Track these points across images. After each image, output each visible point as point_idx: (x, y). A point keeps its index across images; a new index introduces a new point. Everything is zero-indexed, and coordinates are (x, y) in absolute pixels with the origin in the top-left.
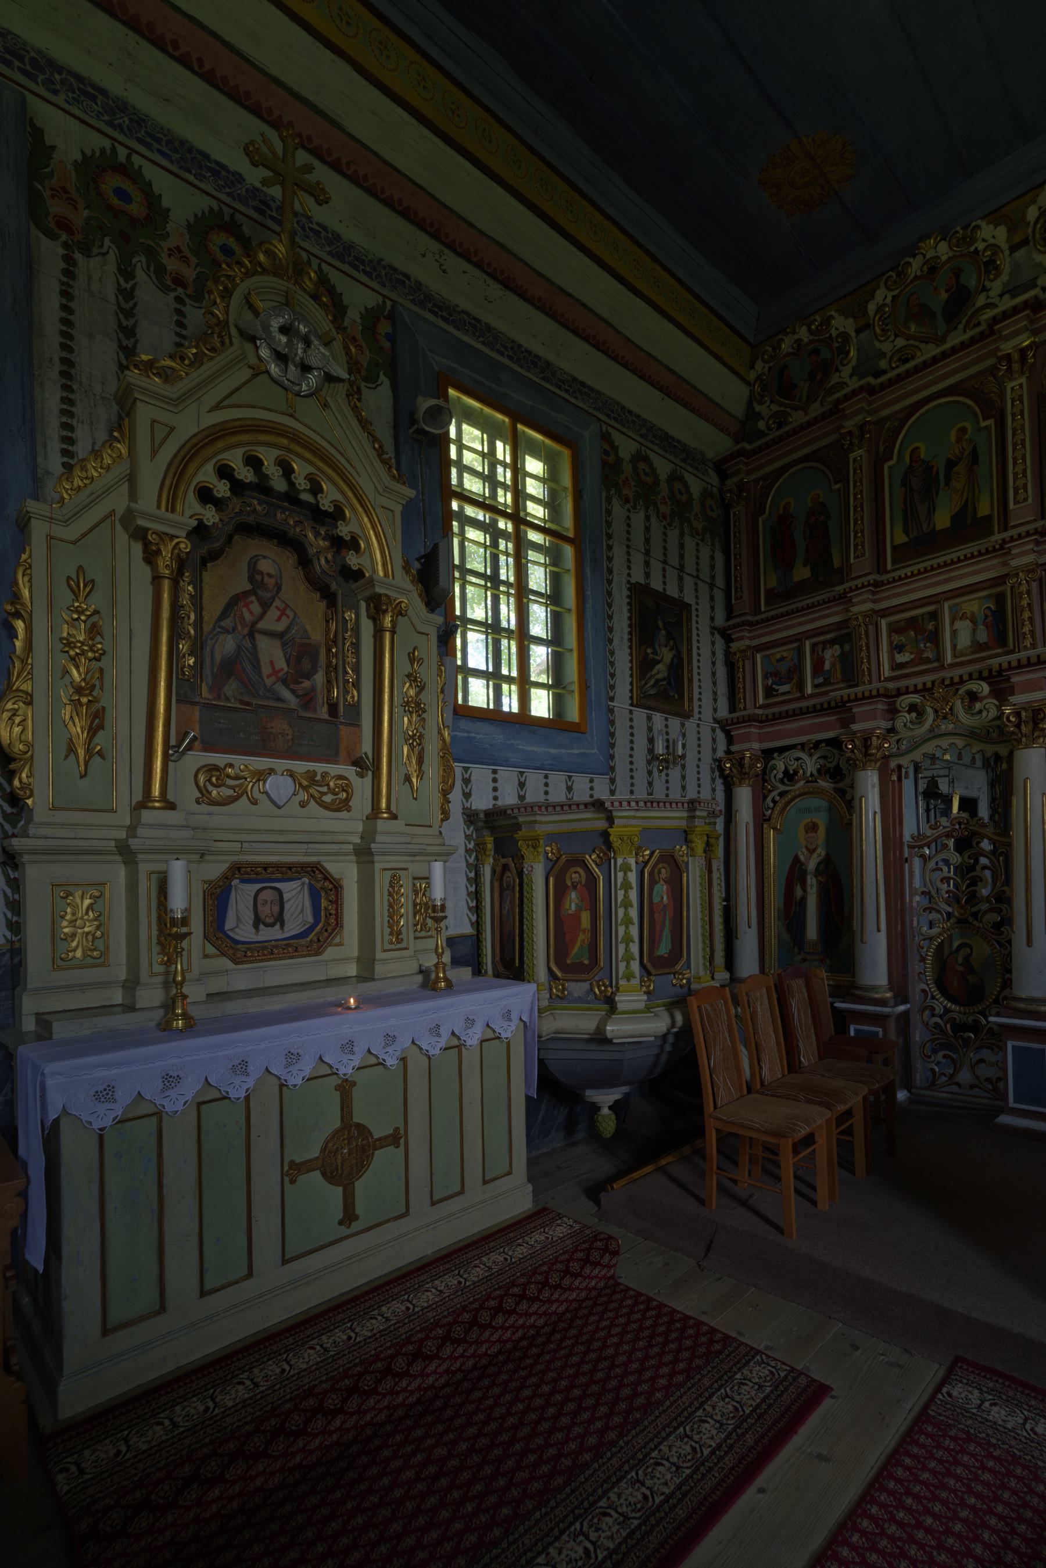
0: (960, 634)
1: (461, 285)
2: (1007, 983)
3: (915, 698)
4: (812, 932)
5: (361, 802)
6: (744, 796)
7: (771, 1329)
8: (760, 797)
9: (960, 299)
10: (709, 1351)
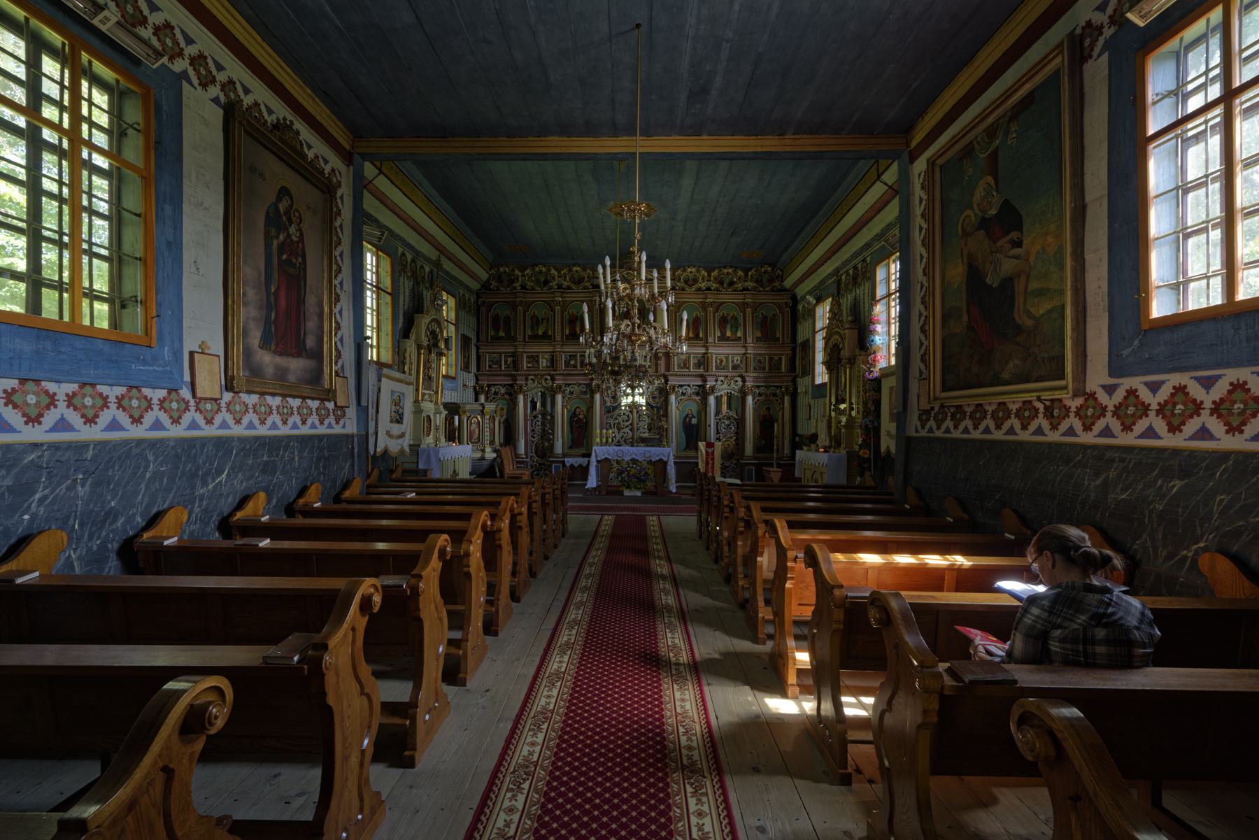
0: (543, 363)
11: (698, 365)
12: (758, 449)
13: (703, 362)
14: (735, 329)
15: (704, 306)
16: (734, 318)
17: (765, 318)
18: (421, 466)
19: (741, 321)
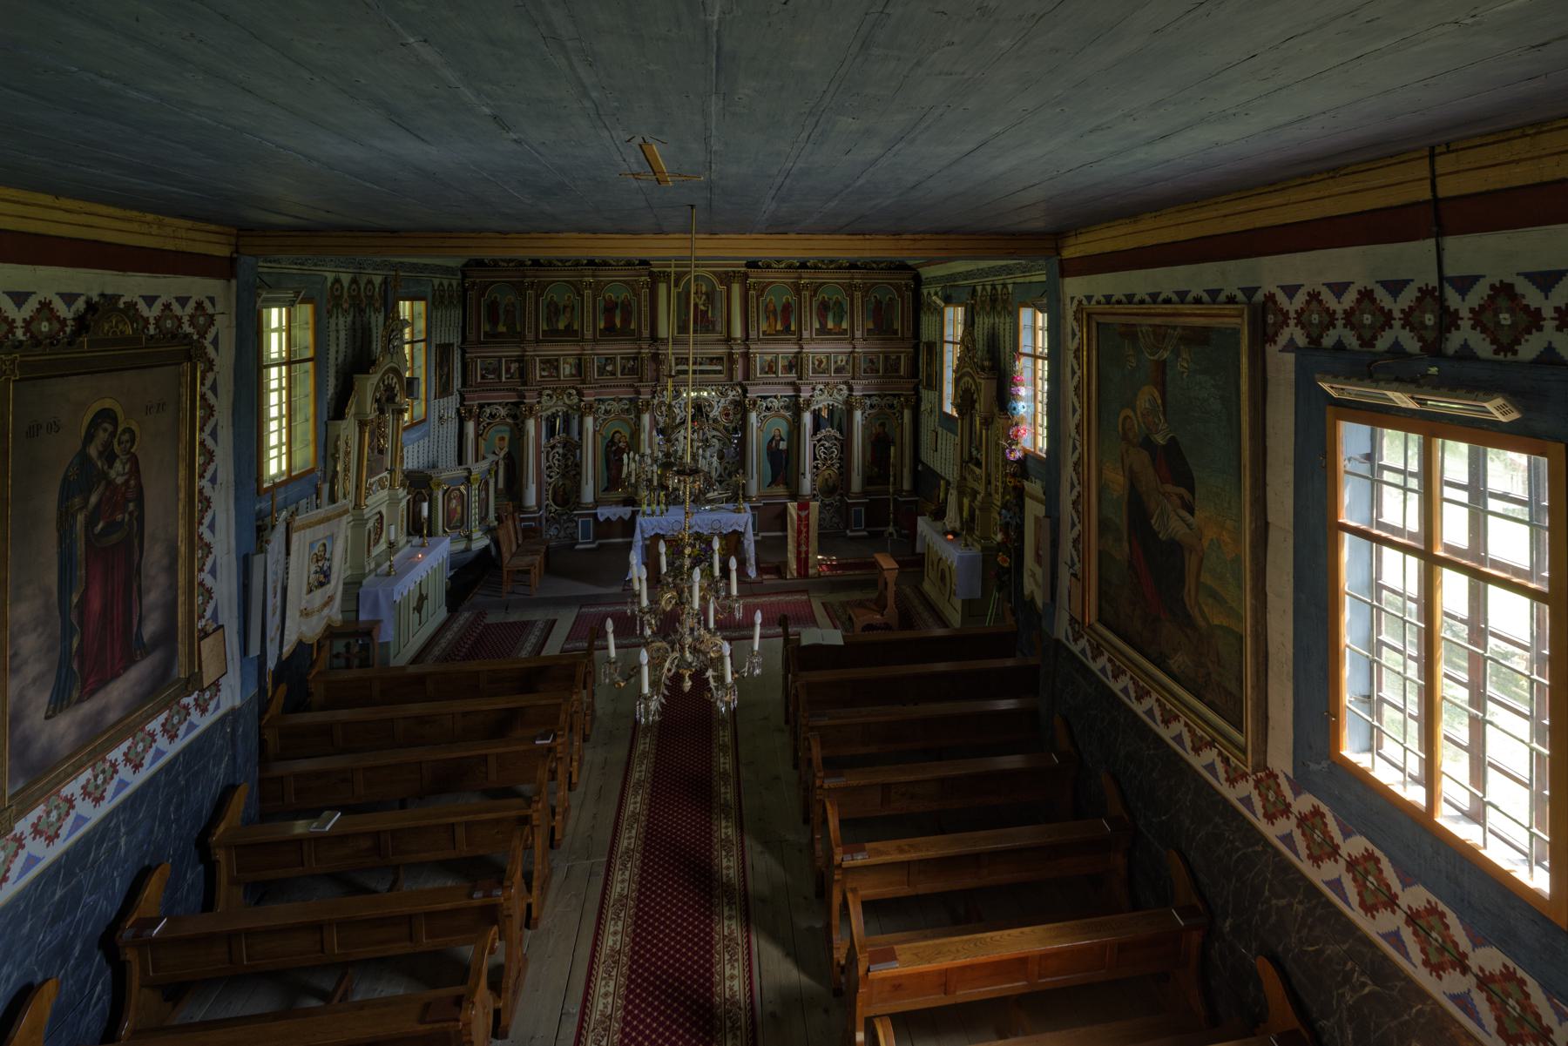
0: (566, 369)
2: (578, 497)
7: (539, 616)
8: (478, 424)
10: (526, 626)
11: (789, 368)
12: (868, 480)
13: (796, 364)
14: (839, 318)
15: (798, 289)
16: (838, 303)
17: (879, 303)
18: (363, 617)
19: (847, 307)
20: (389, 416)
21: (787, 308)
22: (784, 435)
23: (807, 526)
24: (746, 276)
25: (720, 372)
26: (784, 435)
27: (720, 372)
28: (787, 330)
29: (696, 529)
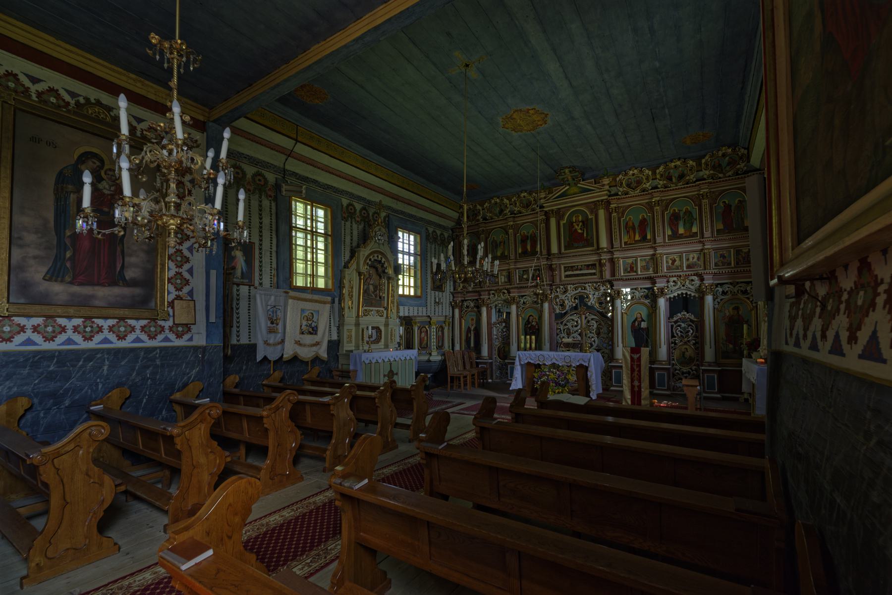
1: (399, 206)
3: (675, 279)
4: (472, 345)
5: (385, 315)
6: (457, 311)
8: (461, 311)
9: (501, 211)
14: (689, 224)
15: (650, 207)
16: (688, 213)
19: (696, 215)
20: (384, 281)
21: (643, 223)
22: (644, 317)
23: (639, 366)
24: (608, 203)
25: (594, 274)
26: (644, 317)
27: (594, 274)
28: (644, 239)
29: (554, 361)
